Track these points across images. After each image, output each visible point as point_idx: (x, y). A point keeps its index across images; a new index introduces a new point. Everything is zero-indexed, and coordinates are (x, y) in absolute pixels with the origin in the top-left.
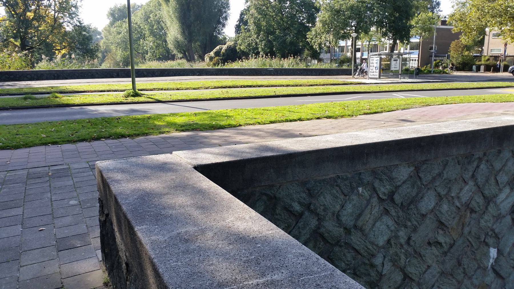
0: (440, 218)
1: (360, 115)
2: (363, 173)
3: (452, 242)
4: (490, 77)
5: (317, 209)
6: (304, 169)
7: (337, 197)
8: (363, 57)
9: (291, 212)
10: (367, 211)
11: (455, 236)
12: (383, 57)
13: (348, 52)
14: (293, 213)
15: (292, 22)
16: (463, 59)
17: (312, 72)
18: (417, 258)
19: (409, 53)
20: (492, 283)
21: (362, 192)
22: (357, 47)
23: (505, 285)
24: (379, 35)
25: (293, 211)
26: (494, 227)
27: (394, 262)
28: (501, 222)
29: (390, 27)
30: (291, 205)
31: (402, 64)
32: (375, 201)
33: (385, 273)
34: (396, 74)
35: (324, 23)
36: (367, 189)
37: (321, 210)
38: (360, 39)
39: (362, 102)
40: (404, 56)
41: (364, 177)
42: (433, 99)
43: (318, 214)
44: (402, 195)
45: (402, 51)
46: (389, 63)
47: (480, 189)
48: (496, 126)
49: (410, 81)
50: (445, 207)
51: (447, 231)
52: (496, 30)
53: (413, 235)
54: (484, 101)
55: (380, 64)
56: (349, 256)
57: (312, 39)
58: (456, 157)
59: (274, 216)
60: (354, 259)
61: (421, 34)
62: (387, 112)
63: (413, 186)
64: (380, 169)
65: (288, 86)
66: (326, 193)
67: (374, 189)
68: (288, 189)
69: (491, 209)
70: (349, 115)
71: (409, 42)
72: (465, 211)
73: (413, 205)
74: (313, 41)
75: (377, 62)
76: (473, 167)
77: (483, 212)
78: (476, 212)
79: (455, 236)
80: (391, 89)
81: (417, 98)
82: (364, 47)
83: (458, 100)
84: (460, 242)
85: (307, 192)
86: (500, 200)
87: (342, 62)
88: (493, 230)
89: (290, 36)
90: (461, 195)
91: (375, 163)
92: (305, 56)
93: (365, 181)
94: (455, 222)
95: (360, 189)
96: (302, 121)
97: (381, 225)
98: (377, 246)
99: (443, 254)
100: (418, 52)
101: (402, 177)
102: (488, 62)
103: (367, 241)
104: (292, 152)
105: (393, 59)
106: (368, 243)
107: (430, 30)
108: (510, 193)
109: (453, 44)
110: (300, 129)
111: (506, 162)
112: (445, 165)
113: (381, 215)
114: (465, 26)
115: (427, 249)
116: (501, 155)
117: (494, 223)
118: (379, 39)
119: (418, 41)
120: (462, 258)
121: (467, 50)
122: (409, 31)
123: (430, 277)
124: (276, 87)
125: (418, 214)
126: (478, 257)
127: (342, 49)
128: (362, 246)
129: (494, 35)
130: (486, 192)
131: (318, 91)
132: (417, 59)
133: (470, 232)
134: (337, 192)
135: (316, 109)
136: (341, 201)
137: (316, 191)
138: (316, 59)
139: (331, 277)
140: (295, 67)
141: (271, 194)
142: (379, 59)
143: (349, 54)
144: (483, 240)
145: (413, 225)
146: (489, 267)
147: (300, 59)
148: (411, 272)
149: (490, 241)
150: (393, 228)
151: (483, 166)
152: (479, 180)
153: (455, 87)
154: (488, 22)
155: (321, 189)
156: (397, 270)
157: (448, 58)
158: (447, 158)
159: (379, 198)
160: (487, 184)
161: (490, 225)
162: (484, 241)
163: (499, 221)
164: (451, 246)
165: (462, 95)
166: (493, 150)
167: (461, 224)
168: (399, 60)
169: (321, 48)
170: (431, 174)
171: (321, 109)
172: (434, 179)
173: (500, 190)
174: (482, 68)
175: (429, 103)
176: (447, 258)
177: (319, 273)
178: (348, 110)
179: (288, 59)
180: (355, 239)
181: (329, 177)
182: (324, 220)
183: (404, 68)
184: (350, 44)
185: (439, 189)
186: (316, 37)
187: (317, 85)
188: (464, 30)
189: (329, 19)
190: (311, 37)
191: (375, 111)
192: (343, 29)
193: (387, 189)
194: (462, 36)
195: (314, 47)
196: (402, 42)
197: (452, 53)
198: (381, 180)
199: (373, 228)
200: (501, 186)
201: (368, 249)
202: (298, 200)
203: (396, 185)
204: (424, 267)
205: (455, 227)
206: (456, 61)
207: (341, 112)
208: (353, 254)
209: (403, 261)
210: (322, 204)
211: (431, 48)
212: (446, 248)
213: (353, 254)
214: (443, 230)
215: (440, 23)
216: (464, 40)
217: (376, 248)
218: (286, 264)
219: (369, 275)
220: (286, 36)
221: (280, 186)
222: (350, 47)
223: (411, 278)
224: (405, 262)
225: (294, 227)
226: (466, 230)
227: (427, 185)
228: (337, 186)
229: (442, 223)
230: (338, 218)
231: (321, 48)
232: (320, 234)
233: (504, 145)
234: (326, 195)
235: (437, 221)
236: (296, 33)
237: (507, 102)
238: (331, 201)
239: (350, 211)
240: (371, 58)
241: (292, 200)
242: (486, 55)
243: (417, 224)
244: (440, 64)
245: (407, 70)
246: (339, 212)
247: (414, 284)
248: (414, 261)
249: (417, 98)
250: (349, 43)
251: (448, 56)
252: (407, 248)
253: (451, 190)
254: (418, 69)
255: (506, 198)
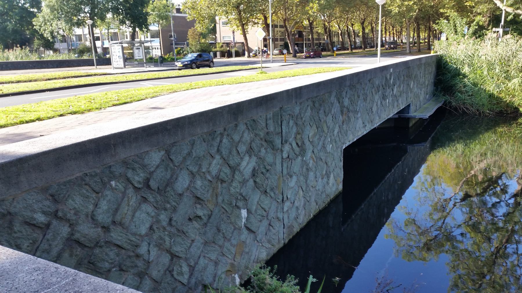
0: (196, 194)
1: (109, 107)
2: (113, 165)
3: (210, 213)
4: (225, 62)
5: (66, 215)
6: (41, 174)
7: (87, 197)
8: (104, 46)
9: (34, 225)
10: (124, 204)
11: (211, 207)
12: (125, 45)
13: (86, 40)
14: (37, 225)
15: (9, 6)
16: (201, 46)
17: (47, 64)
18: (180, 236)
19: (151, 41)
20: (246, 239)
21: (115, 185)
22: (95, 35)
23: (256, 238)
24: (117, 23)
25: (37, 223)
26: (242, 191)
27: (159, 246)
28: (246, 186)
29: (127, 14)
30: (33, 218)
31: (145, 52)
32: (130, 191)
33: (152, 259)
34: (141, 63)
35: (52, 9)
36: (120, 181)
37: (72, 215)
38: (98, 27)
39: (109, 94)
40: (146, 45)
41: (115, 170)
42: (178, 85)
43: (69, 220)
44: (157, 180)
45: (143, 39)
46: (131, 51)
47: (226, 161)
48: (230, 104)
49: (156, 70)
50: (199, 183)
51: (203, 204)
52: (224, 19)
53: (173, 215)
54: (222, 84)
55: (123, 54)
56: (112, 255)
57: (40, 26)
58: (201, 135)
59: (13, 235)
60: (118, 256)
61: (159, 22)
62: (137, 101)
63: (166, 170)
64: (131, 158)
65: (18, 82)
66: (75, 195)
67: (128, 180)
68: (25, 200)
69: (238, 177)
70: (97, 109)
71: (148, 30)
72: (217, 183)
73: (170, 187)
74: (42, 28)
75: (119, 50)
76: (217, 142)
77: (231, 181)
78: (225, 182)
79: (211, 207)
80: (138, 78)
81: (164, 86)
82: (103, 35)
83: (201, 84)
84: (217, 211)
85: (51, 198)
86: (243, 167)
87: (82, 52)
88: (241, 194)
89: (11, 22)
90: (211, 169)
91: (123, 154)
92: (35, 47)
93: (116, 173)
94: (209, 194)
95: (113, 183)
96: (41, 120)
97: (140, 214)
98: (140, 235)
99: (203, 225)
100: (159, 41)
101: (154, 163)
102: (222, 49)
103: (128, 234)
104: (22, 156)
105: (135, 48)
106: (130, 235)
107: (166, 18)
108: (249, 160)
109: (190, 32)
110: (41, 129)
111: (243, 134)
112: (193, 144)
113: (140, 204)
114: (197, 14)
115: (188, 225)
116: (238, 128)
117: (241, 188)
118: (118, 27)
119: (157, 29)
120: (220, 225)
121: (203, 38)
122: (146, 19)
123: (196, 250)
124: (3, 85)
125: (175, 194)
126: (233, 220)
127: (79, 38)
128: (124, 240)
129: (223, 23)
130: (231, 163)
131: (58, 86)
132: (159, 47)
133: (224, 200)
134: (87, 191)
135: (57, 105)
136: (94, 199)
137: (62, 195)
138: (51, 49)
139: (73, 283)
140: (25, 59)
141: (2, 211)
142: (120, 47)
143: (88, 44)
144: (234, 204)
145: (172, 206)
146: (243, 226)
147: (30, 50)
148: (177, 250)
149: (240, 204)
150: (153, 214)
151: (225, 140)
152: (224, 153)
153: (197, 73)
154: (217, 10)
155: (67, 191)
156: (164, 253)
157: (187, 46)
158: (193, 138)
159: (135, 188)
160: (231, 156)
161: (238, 191)
162: (236, 205)
163: (245, 185)
164: (210, 217)
165: (204, 80)
166: (231, 125)
167: (214, 195)
168: (141, 48)
169: (53, 37)
170: (182, 155)
171: (63, 105)
172: (185, 159)
173: (242, 159)
174: (218, 54)
175: (175, 89)
176: (208, 228)
177: (59, 282)
178: (95, 103)
179: (14, 50)
180: (116, 235)
181: (74, 177)
182: (77, 225)
183: (148, 56)
184: (88, 33)
185: (190, 168)
186: (46, 24)
187: (55, 79)
188: (198, 18)
189: (57, 3)
190: (39, 24)
191: (124, 101)
192: (76, 16)
193: (141, 177)
194: (197, 24)
195: (45, 35)
196: (141, 29)
197: (190, 41)
198: (133, 169)
199: (133, 219)
200: (242, 155)
201: (131, 241)
202: (40, 210)
203: (150, 171)
204: (188, 243)
205: (210, 199)
206: (195, 48)
207: (87, 106)
208: (116, 251)
209: (167, 243)
210: (71, 208)
211: (171, 36)
212: (205, 219)
213: (116, 251)
214: (200, 204)
215: (175, 12)
216: (199, 28)
217: (139, 238)
218: (16, 286)
219: (136, 266)
220: (5, 22)
221: (13, 199)
222: (88, 36)
223: (178, 257)
224: (171, 243)
225: (42, 241)
226: (220, 199)
227: (179, 166)
228: (86, 184)
229: (198, 198)
230: (92, 219)
231: (53, 37)
232: (75, 241)
233: (239, 120)
234: (74, 197)
235: (193, 197)
236: (18, 20)
237: (241, 83)
238: (82, 203)
239: (105, 208)
240: (112, 47)
241: (34, 211)
242: (219, 42)
243: (175, 204)
244: (181, 51)
245: (151, 58)
246: (93, 212)
247: (182, 261)
248: (179, 239)
249: (164, 86)
250: (86, 30)
251: (187, 43)
252: (169, 230)
253: (202, 167)
254: (161, 57)
255: (248, 164)
